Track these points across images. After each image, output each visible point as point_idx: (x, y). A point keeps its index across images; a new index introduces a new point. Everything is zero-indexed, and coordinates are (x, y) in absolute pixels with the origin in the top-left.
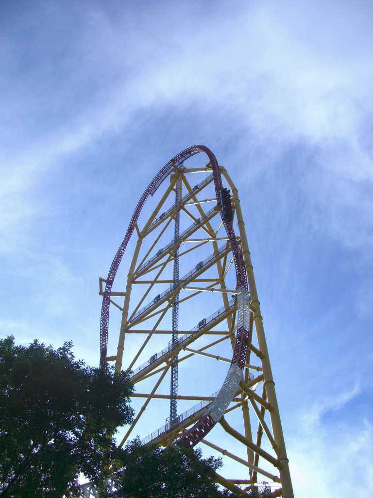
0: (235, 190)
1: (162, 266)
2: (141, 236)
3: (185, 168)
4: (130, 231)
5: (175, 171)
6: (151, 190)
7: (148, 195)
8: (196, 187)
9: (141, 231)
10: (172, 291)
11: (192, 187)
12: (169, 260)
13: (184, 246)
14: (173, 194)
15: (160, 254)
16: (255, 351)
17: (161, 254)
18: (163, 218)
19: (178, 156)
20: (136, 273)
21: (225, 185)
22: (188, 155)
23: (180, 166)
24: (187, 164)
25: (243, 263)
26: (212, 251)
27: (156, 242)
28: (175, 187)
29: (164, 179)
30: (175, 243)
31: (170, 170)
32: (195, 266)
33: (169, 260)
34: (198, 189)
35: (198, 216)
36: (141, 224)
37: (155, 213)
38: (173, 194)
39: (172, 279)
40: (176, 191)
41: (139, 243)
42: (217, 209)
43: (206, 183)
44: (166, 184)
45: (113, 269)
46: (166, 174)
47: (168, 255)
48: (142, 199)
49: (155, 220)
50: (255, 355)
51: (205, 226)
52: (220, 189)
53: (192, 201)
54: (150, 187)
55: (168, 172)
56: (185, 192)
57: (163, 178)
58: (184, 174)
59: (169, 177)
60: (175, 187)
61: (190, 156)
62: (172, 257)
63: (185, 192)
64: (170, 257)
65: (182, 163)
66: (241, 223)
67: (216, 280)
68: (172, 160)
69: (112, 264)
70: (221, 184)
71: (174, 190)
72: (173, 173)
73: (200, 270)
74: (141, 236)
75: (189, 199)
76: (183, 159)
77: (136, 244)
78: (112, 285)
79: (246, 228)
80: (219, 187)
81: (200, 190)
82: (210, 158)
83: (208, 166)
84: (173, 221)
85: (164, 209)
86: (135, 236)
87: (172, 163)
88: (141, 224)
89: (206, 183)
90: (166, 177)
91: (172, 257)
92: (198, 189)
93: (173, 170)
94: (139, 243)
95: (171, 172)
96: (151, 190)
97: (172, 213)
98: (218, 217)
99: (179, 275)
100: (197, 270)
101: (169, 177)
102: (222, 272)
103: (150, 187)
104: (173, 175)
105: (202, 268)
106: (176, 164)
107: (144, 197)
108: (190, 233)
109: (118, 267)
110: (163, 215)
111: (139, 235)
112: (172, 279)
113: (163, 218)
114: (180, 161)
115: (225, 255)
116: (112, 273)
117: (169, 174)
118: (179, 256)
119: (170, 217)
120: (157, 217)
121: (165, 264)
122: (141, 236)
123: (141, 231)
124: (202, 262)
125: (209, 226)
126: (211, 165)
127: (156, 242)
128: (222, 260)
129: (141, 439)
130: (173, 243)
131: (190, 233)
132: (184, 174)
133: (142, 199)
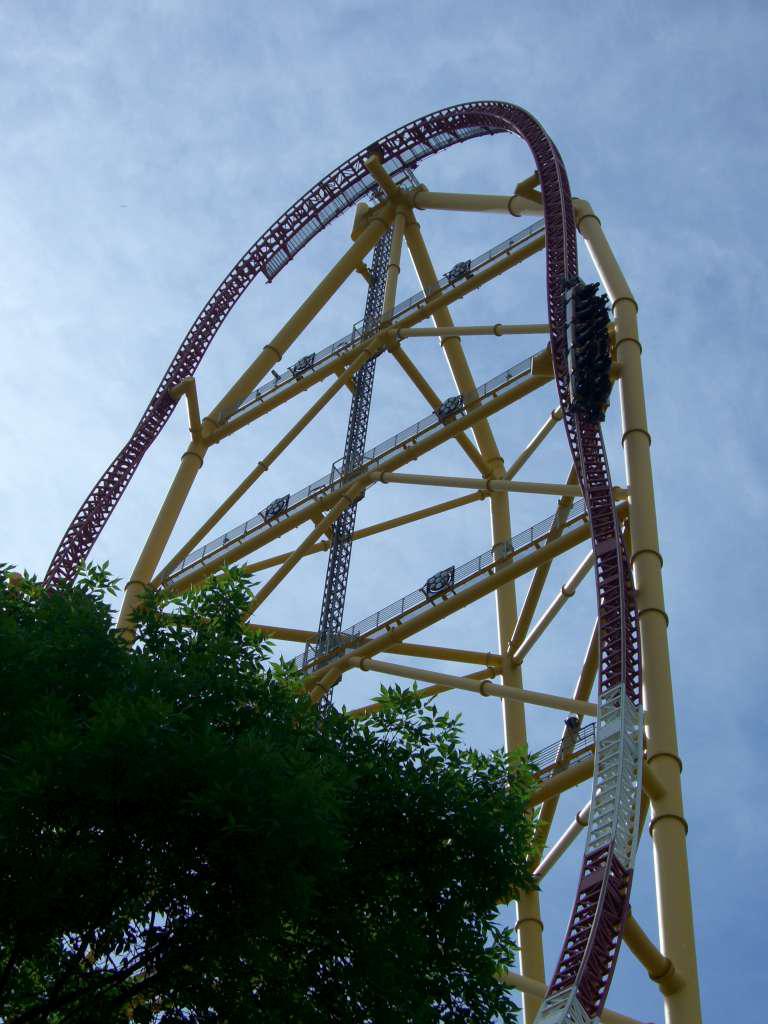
0: (626, 300)
1: (274, 570)
2: (208, 432)
3: (421, 188)
4: (162, 405)
5: (378, 195)
6: (263, 261)
7: (255, 274)
8: (463, 271)
9: (205, 412)
10: (310, 671)
11: (442, 267)
12: (308, 548)
13: (376, 503)
14: (356, 287)
15: (276, 515)
16: (643, 949)
17: (279, 517)
18: (305, 374)
19: (401, 136)
20: (165, 576)
21: (589, 268)
22: (445, 137)
23: (401, 176)
24: (441, 171)
25: (631, 597)
26: (483, 540)
27: (263, 467)
28: (368, 260)
29: (329, 221)
30: (343, 480)
31: (358, 188)
32: (422, 583)
33: (308, 548)
34: (467, 278)
35: (448, 388)
36: (213, 382)
37: (274, 351)
38: (356, 287)
39: (314, 626)
40: (373, 280)
41: (192, 461)
42: (545, 367)
43: (510, 258)
44: (337, 237)
45: (73, 546)
46: (341, 200)
47: (308, 528)
48: (229, 285)
49: (269, 378)
50: (642, 971)
51: (470, 433)
52: (568, 286)
53: (432, 322)
54: (266, 244)
55: (350, 193)
56: (409, 284)
57: (324, 215)
58: (414, 210)
59: (350, 215)
60: (368, 260)
61: (450, 143)
62: (324, 537)
63: (409, 284)
64: (315, 536)
65: (413, 165)
66: (637, 435)
67: (485, 658)
68: (374, 149)
69: (73, 527)
70: (573, 268)
71: (363, 270)
72: (369, 202)
73: (439, 601)
74: (205, 434)
75: (423, 315)
76: (418, 149)
77: (176, 464)
78: (175, 406)
79: (657, 452)
80: (562, 274)
81: (476, 283)
82: (538, 160)
83: (524, 190)
84: (345, 395)
85: (317, 339)
86: (175, 435)
87: (373, 157)
88: (213, 382)
89: (510, 258)
90: (339, 212)
91: (324, 537)
92: (467, 278)
93: (373, 187)
94: (192, 461)
95: (360, 195)
96: (263, 261)
97: (347, 359)
98: (548, 398)
99: (346, 610)
100: (430, 600)
101: (350, 215)
102: (517, 628)
103: (266, 244)
104: (371, 211)
105: (450, 595)
106: (390, 166)
107: (235, 278)
108: (413, 448)
109: (93, 541)
110: (308, 363)
111: (195, 428)
112: (314, 626)
113: (305, 374)
114: (407, 156)
115: (541, 561)
116: (68, 565)
117: (350, 204)
118: (351, 538)
119: (333, 379)
120: (283, 367)
121: (289, 562)
122: (205, 434)
123: (205, 412)
124: (452, 570)
125: (485, 436)
126: (538, 188)
127: (263, 467)
128: (523, 585)
129: (540, 893)
130: (337, 478)
131: (413, 448)
132: (414, 210)
133: (229, 285)
